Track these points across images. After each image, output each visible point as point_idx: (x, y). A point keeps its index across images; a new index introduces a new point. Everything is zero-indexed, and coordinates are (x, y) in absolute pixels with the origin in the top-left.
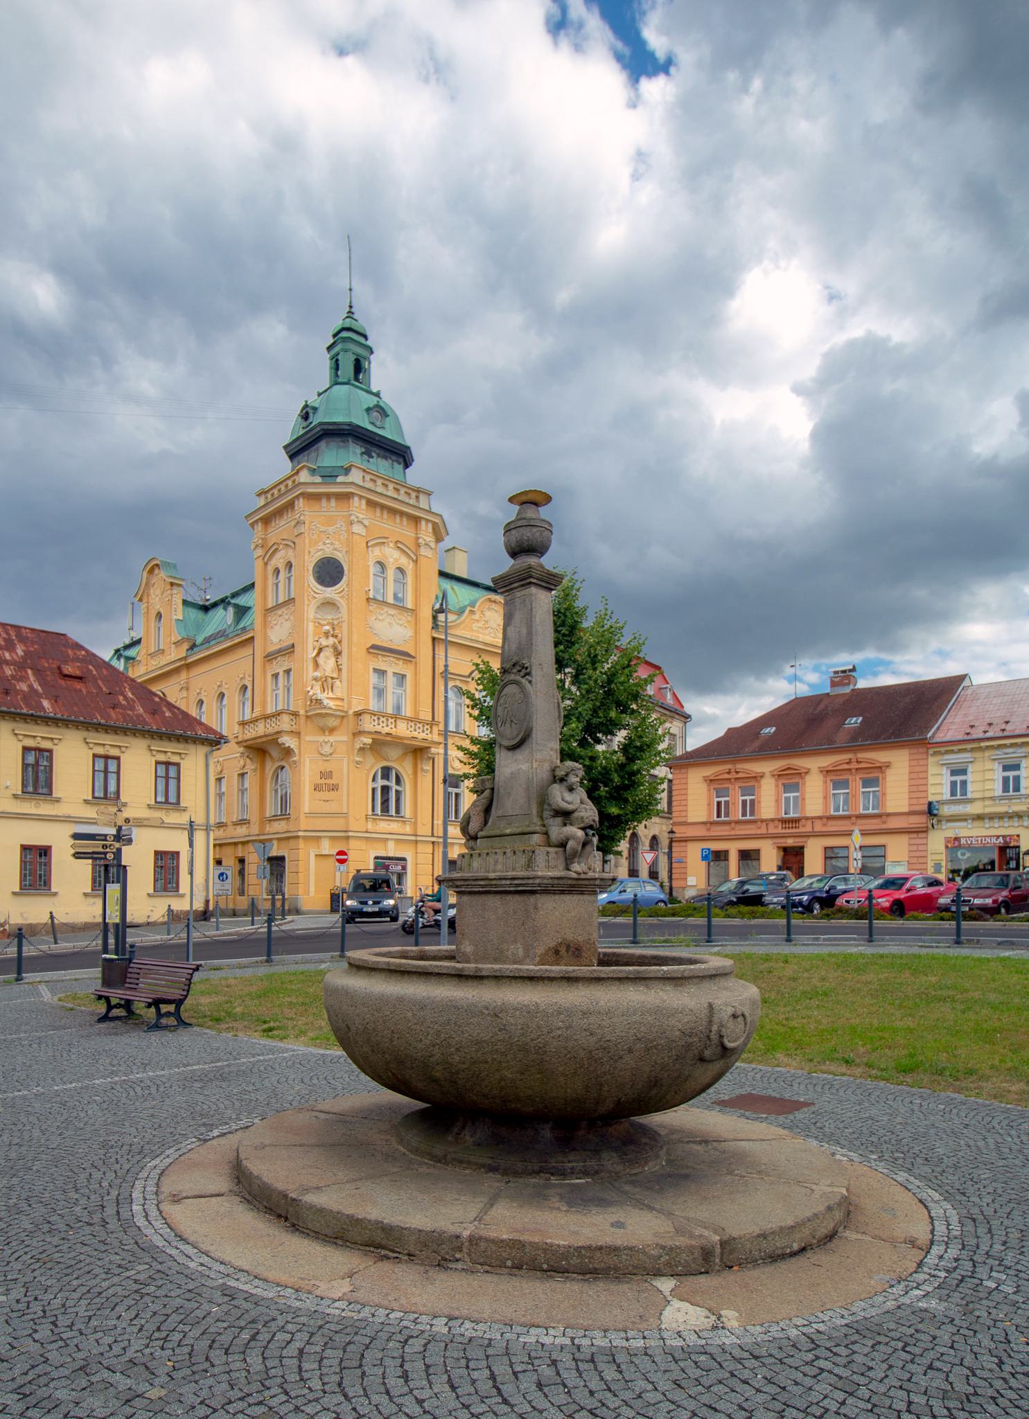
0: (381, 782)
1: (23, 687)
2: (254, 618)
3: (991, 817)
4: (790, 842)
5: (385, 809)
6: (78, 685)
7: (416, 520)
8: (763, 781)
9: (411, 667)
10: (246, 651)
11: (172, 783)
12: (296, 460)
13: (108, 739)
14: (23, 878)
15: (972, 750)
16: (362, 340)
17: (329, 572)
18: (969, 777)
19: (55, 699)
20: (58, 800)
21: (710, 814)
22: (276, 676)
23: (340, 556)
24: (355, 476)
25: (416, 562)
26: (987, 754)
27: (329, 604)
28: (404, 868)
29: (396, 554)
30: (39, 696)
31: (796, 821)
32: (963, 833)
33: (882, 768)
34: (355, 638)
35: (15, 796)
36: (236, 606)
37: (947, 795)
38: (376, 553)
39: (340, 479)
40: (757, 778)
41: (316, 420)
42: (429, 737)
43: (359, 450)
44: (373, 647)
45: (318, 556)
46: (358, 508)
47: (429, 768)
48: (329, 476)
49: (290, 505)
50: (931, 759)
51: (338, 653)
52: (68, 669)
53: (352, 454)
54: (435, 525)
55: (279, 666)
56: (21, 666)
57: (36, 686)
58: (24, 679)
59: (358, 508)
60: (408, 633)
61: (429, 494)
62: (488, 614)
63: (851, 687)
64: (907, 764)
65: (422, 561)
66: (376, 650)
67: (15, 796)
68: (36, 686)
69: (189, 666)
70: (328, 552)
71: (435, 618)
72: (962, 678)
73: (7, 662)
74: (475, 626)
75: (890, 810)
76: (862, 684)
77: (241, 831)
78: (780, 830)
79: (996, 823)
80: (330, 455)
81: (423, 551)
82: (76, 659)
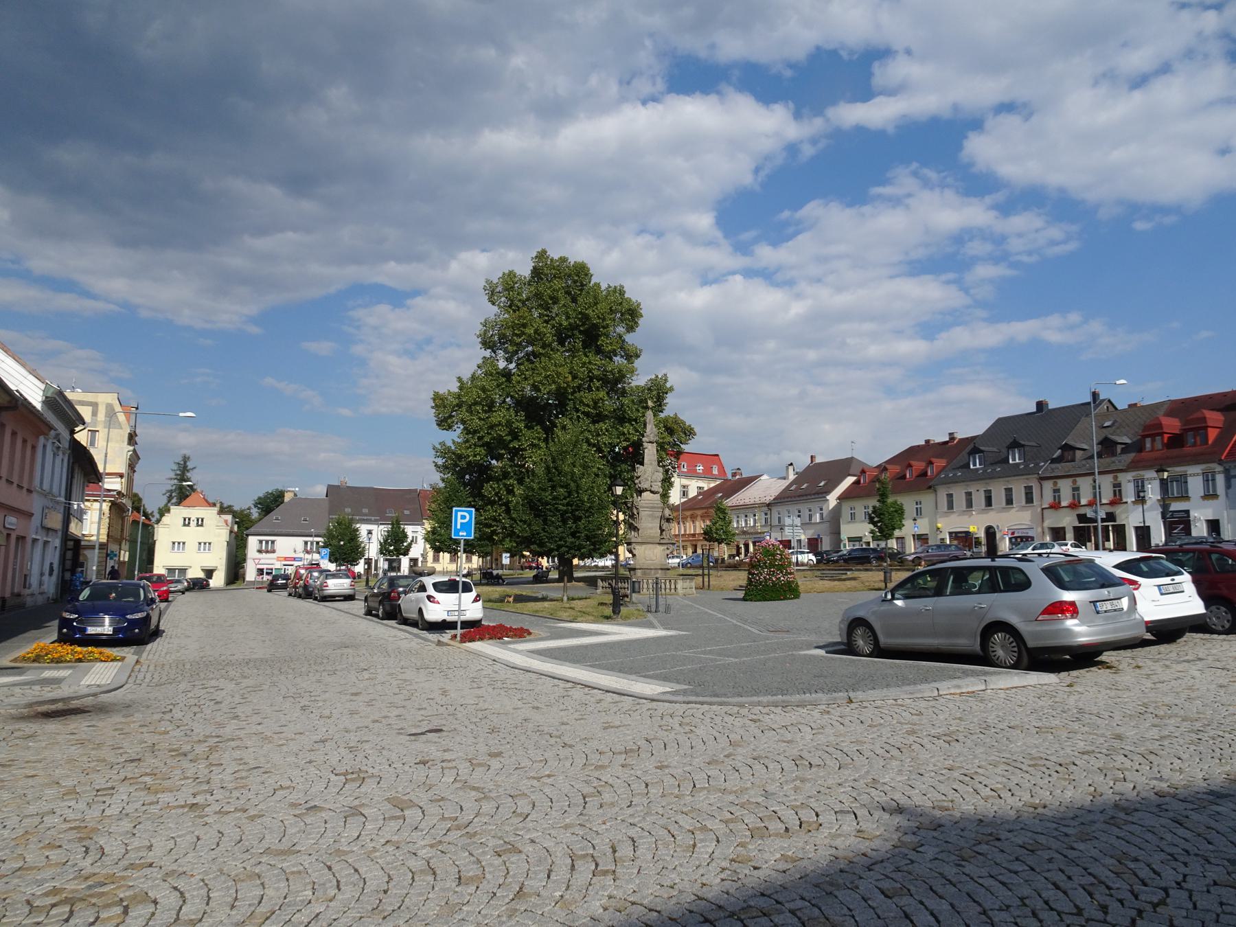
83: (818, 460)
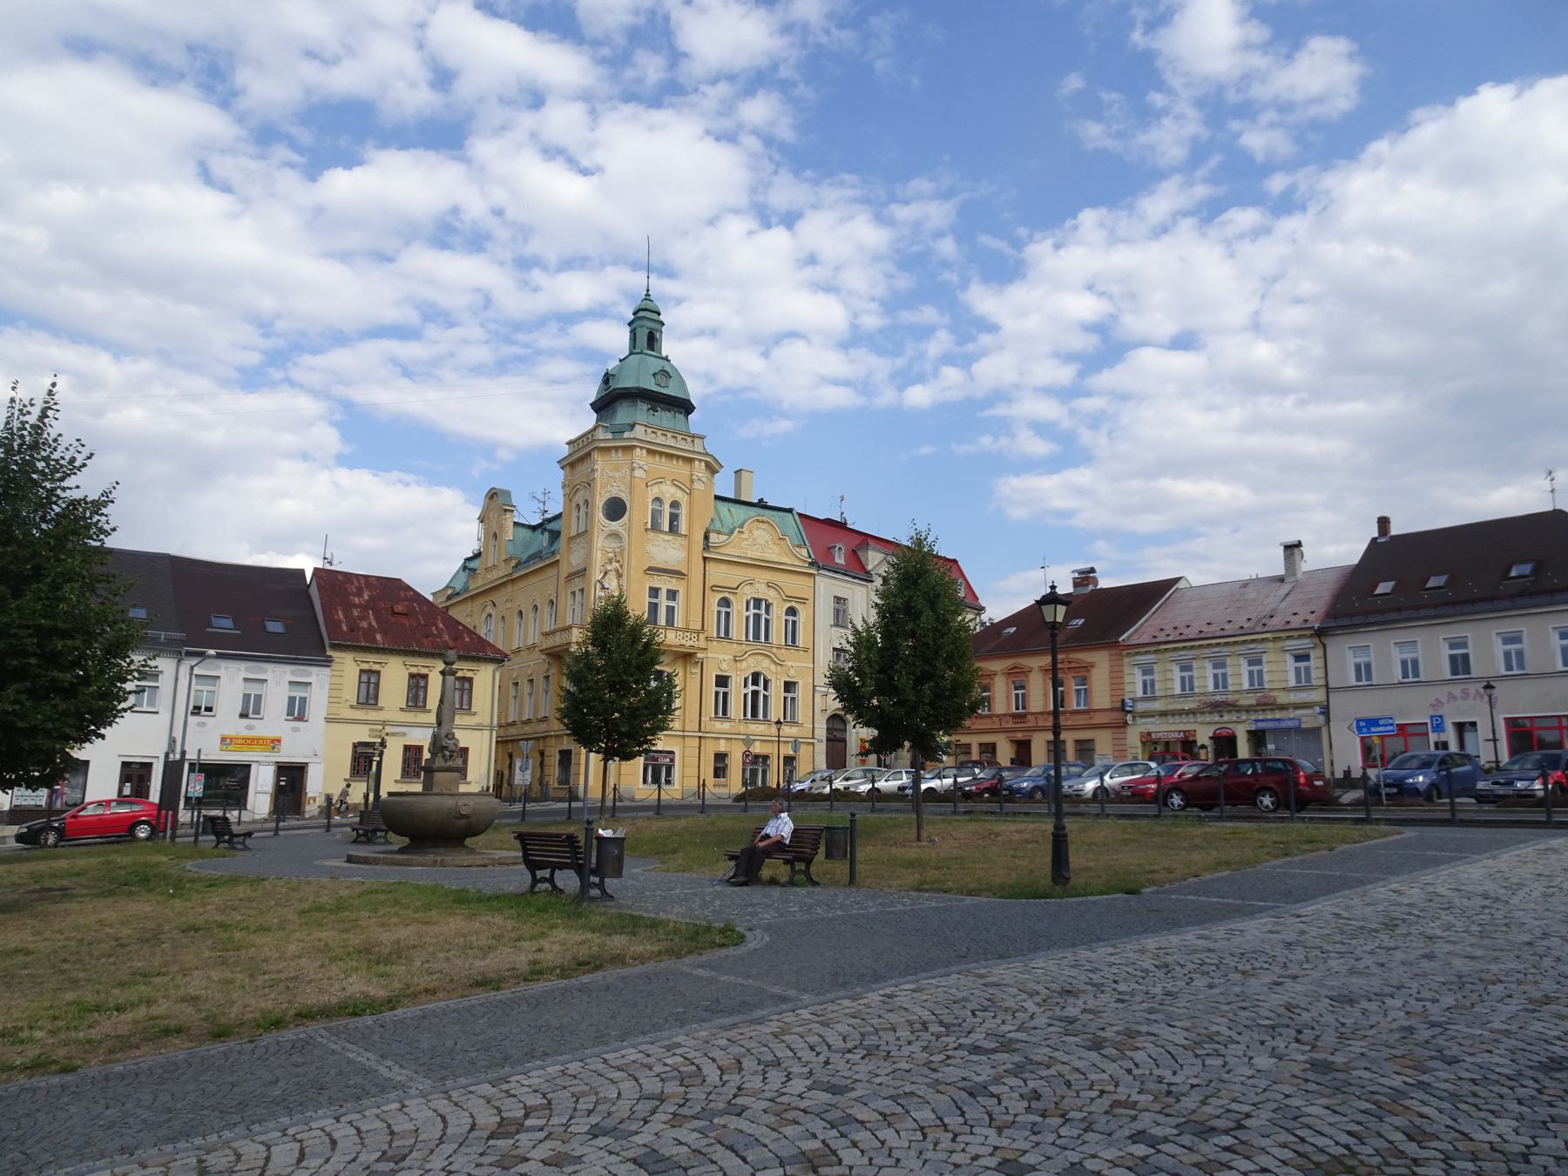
0: (752, 611)
1: (364, 624)
2: (562, 543)
3: (1174, 713)
4: (1019, 736)
5: (757, 636)
6: (404, 621)
7: (690, 461)
8: (1031, 676)
9: (684, 583)
10: (552, 572)
11: (465, 697)
12: (604, 413)
13: (420, 661)
14: (404, 770)
15: (1155, 652)
16: (655, 316)
17: (616, 509)
18: (1525, 645)
19: (385, 633)
20: (381, 709)
21: (1009, 706)
22: (573, 593)
23: (623, 496)
24: (639, 432)
25: (690, 494)
26: (1167, 655)
27: (615, 535)
28: (672, 760)
29: (673, 489)
30: (375, 631)
31: (1023, 716)
32: (1152, 728)
33: (1088, 667)
34: (633, 562)
35: (352, 707)
36: (551, 531)
37: (1140, 694)
38: (655, 491)
39: (626, 435)
40: (992, 675)
41: (614, 385)
42: (696, 644)
43: (645, 407)
44: (650, 569)
45: (608, 496)
46: (640, 455)
47: (698, 670)
48: (618, 432)
49: (588, 455)
50: (1127, 660)
51: (620, 576)
52: (399, 608)
53: (641, 412)
54: (708, 465)
55: (577, 584)
56: (365, 608)
57: (374, 624)
58: (365, 618)
59: (640, 455)
60: (682, 554)
61: (702, 438)
62: (756, 533)
63: (1091, 587)
64: (1107, 664)
65: (696, 494)
66: (653, 570)
67: (352, 707)
68: (374, 624)
69: (513, 581)
70: (615, 492)
71: (706, 537)
72: (1177, 580)
73: (356, 606)
74: (744, 544)
75: (1096, 707)
76: (1104, 583)
77: (543, 727)
78: (1011, 725)
79: (1177, 719)
80: (623, 414)
81: (697, 485)
82: (406, 599)
83: (1395, 530)
